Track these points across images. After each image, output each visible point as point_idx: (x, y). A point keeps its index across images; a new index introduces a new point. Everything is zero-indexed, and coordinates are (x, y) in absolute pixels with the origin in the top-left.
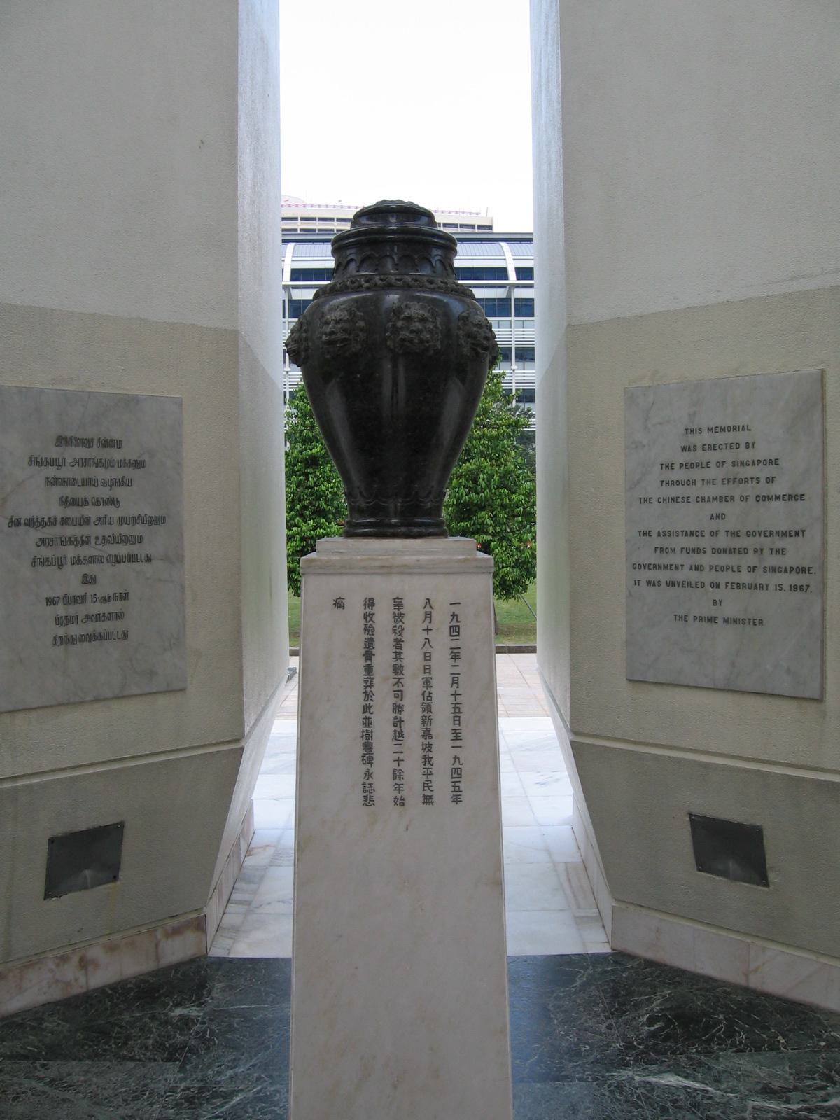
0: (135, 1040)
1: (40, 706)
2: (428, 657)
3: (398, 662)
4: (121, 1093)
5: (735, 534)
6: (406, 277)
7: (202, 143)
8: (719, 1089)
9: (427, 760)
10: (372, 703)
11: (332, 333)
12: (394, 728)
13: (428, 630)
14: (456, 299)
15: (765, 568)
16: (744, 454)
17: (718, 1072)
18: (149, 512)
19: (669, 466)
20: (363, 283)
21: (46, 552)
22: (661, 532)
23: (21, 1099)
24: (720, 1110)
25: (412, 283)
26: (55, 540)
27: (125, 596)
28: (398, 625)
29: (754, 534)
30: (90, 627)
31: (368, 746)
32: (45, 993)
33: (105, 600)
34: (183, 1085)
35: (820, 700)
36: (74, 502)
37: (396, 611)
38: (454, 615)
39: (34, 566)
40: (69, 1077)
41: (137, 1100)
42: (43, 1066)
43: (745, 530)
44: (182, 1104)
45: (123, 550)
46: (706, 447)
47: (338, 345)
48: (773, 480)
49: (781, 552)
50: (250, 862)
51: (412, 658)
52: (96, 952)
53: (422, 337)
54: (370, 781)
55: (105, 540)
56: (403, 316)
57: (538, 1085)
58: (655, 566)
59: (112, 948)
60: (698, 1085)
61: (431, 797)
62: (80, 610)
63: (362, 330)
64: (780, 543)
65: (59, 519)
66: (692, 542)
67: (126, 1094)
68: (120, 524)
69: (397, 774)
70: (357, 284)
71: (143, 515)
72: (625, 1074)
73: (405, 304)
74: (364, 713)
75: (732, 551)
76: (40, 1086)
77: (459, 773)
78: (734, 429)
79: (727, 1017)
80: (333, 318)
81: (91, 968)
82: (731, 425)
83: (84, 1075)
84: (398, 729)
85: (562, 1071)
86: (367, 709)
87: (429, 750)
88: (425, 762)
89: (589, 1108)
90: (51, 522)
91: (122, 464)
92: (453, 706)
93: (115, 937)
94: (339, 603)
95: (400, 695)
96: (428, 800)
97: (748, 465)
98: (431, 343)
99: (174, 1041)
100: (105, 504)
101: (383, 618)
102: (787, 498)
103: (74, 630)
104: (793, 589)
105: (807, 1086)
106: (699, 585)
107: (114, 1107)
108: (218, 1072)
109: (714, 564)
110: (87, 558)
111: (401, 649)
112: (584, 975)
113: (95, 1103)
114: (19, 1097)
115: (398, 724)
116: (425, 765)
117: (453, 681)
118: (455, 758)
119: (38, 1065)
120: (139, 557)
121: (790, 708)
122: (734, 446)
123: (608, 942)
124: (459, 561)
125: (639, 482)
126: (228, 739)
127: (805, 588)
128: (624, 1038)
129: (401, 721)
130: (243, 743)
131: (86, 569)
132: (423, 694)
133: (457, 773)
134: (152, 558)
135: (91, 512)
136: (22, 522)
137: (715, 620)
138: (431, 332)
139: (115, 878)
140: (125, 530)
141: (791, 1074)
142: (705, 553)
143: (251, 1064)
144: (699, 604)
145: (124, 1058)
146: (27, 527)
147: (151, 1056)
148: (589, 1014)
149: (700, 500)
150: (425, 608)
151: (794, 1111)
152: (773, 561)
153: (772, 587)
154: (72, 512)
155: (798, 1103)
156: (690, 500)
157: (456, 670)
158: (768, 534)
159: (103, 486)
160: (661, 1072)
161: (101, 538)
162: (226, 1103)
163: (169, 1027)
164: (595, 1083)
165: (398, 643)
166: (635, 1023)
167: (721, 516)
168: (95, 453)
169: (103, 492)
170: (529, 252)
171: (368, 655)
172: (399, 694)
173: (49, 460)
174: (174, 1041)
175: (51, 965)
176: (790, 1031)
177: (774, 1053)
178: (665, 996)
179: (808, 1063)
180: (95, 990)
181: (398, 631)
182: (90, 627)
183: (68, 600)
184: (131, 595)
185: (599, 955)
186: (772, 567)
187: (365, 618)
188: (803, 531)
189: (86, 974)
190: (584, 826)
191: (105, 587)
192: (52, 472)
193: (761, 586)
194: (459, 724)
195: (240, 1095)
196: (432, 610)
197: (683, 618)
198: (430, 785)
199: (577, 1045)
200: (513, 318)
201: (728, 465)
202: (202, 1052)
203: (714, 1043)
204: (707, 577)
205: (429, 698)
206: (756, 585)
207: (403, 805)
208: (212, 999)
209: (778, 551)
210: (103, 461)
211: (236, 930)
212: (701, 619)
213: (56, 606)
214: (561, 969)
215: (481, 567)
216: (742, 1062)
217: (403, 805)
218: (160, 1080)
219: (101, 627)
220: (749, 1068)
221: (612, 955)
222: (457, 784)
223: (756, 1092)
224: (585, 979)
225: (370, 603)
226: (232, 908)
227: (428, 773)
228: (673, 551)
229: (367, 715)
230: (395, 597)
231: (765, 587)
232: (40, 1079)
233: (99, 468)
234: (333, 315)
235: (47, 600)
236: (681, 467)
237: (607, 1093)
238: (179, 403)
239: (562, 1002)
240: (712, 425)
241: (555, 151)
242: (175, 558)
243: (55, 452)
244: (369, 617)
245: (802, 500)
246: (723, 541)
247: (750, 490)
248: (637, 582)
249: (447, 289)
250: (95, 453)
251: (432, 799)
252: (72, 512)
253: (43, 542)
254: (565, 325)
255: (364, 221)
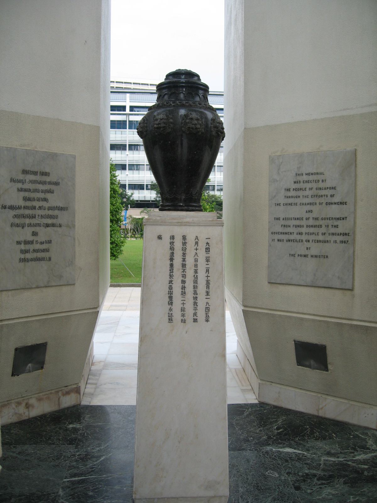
0: (54, 437)
1: (13, 289)
2: (196, 260)
3: (184, 263)
4: (51, 457)
5: (317, 219)
6: (189, 102)
7: (86, 42)
8: (309, 453)
9: (195, 304)
10: (173, 280)
11: (159, 124)
12: (181, 290)
13: (196, 249)
14: (210, 112)
15: (329, 233)
16: (321, 185)
17: (308, 447)
18: (61, 205)
19: (288, 190)
20: (172, 103)
21: (17, 221)
22: (284, 218)
23: (7, 460)
24: (310, 461)
25: (192, 104)
26: (22, 215)
27: (50, 242)
28: (184, 247)
29: (325, 219)
30: (35, 255)
31: (171, 298)
32: (11, 419)
33: (42, 243)
34: (78, 454)
35: (352, 290)
36: (29, 199)
37: (184, 241)
38: (207, 243)
39: (12, 227)
40: (26, 451)
41: (59, 459)
42: (14, 447)
43: (321, 218)
44: (79, 461)
45: (49, 221)
46: (305, 182)
47: (162, 129)
48: (333, 196)
49: (336, 226)
50: (93, 368)
51: (190, 261)
52: (33, 401)
53: (197, 127)
54: (171, 312)
55: (42, 217)
56: (189, 118)
57: (232, 452)
58: (281, 233)
59: (39, 400)
60: (300, 452)
61: (196, 319)
62: (31, 247)
63: (172, 123)
64: (336, 223)
65: (23, 207)
66: (297, 223)
67: (53, 457)
68: (49, 210)
69: (183, 310)
70: (169, 104)
71: (58, 206)
72: (269, 448)
73: (190, 113)
74: (169, 283)
75: (315, 226)
76: (15, 455)
77: (208, 309)
78: (317, 174)
79: (310, 427)
80: (160, 118)
81: (30, 408)
82: (316, 172)
83: (33, 450)
84: (183, 290)
85: (242, 447)
86: (171, 282)
87: (196, 300)
88: (194, 304)
89: (254, 460)
90: (19, 208)
91: (50, 183)
92: (207, 281)
93: (41, 394)
94: (160, 237)
95: (184, 276)
96: (195, 320)
97: (323, 189)
98: (200, 130)
99: (71, 437)
100: (42, 200)
101: (178, 245)
102: (339, 203)
103: (28, 256)
104: (341, 242)
105: (345, 452)
106: (300, 241)
107: (49, 462)
108: (92, 448)
109: (307, 232)
110: (34, 224)
111: (185, 257)
112: (247, 411)
113: (40, 461)
114: (6, 459)
115: (184, 288)
116: (194, 306)
117: (207, 271)
118: (207, 303)
119: (12, 447)
120: (56, 225)
121: (338, 292)
122: (317, 181)
123: (257, 399)
124: (210, 221)
125: (275, 196)
126: (92, 307)
127: (346, 242)
128: (267, 435)
129: (185, 287)
130: (98, 309)
131: (34, 229)
132: (194, 276)
133: (207, 309)
134: (62, 225)
135: (37, 204)
136: (7, 207)
137: (307, 256)
138: (200, 125)
139: (42, 368)
140: (51, 212)
141: (339, 448)
142: (303, 227)
143: (106, 445)
144: (301, 249)
145: (50, 444)
146: (9, 209)
147: (62, 443)
148: (251, 426)
149: (302, 204)
150: (195, 240)
151: (341, 461)
152: (333, 230)
153: (332, 242)
154: (29, 204)
155: (343, 458)
156: (297, 204)
157: (208, 266)
158: (331, 219)
159: (42, 192)
160: (284, 447)
161: (40, 216)
162: (98, 460)
163: (68, 432)
164: (256, 451)
165: (184, 254)
166: (271, 429)
167: (311, 211)
168: (38, 178)
169: (41, 195)
170: (213, 100)
171: (172, 259)
172: (184, 276)
173: (19, 180)
174: (71, 437)
175: (14, 406)
176: (337, 432)
177: (331, 440)
178: (283, 419)
179: (346, 443)
180: (33, 418)
181: (184, 250)
182: (35, 255)
183: (26, 242)
184: (52, 241)
185: (253, 404)
186: (315, 256)
187: (170, 244)
188: (346, 218)
189: (29, 411)
190: (244, 352)
191: (42, 237)
192: (20, 185)
193: (328, 241)
194: (209, 289)
195: (104, 457)
196: (198, 241)
197: (293, 255)
198: (196, 314)
199: (247, 437)
200: (128, 130)
201: (314, 189)
202: (84, 441)
203: (305, 436)
204: (304, 237)
205: (197, 278)
206: (325, 241)
207: (185, 323)
208: (85, 421)
209: (335, 226)
210: (42, 181)
211: (92, 395)
212: (301, 256)
213: (21, 245)
214: (236, 411)
215: (219, 224)
216: (318, 443)
217: (185, 323)
218: (67, 452)
219: (40, 255)
220: (321, 445)
221: (259, 404)
222: (208, 314)
223: (325, 454)
224: (248, 413)
225: (173, 237)
226: (88, 386)
227: (195, 309)
228: (289, 226)
229: (171, 284)
230: (183, 235)
231: (329, 242)
232: (14, 452)
233: (40, 185)
234: (159, 116)
235: (17, 242)
236: (293, 190)
237: (262, 455)
238: (74, 157)
239: (239, 422)
240: (307, 172)
241: (239, 51)
242: (71, 226)
243: (21, 177)
244: (172, 243)
245: (346, 204)
246: (311, 222)
247: (323, 200)
248: (273, 240)
249: (206, 107)
250: (38, 178)
251: (197, 320)
252: (29, 204)
253: (16, 216)
254: (243, 128)
255: (171, 77)
